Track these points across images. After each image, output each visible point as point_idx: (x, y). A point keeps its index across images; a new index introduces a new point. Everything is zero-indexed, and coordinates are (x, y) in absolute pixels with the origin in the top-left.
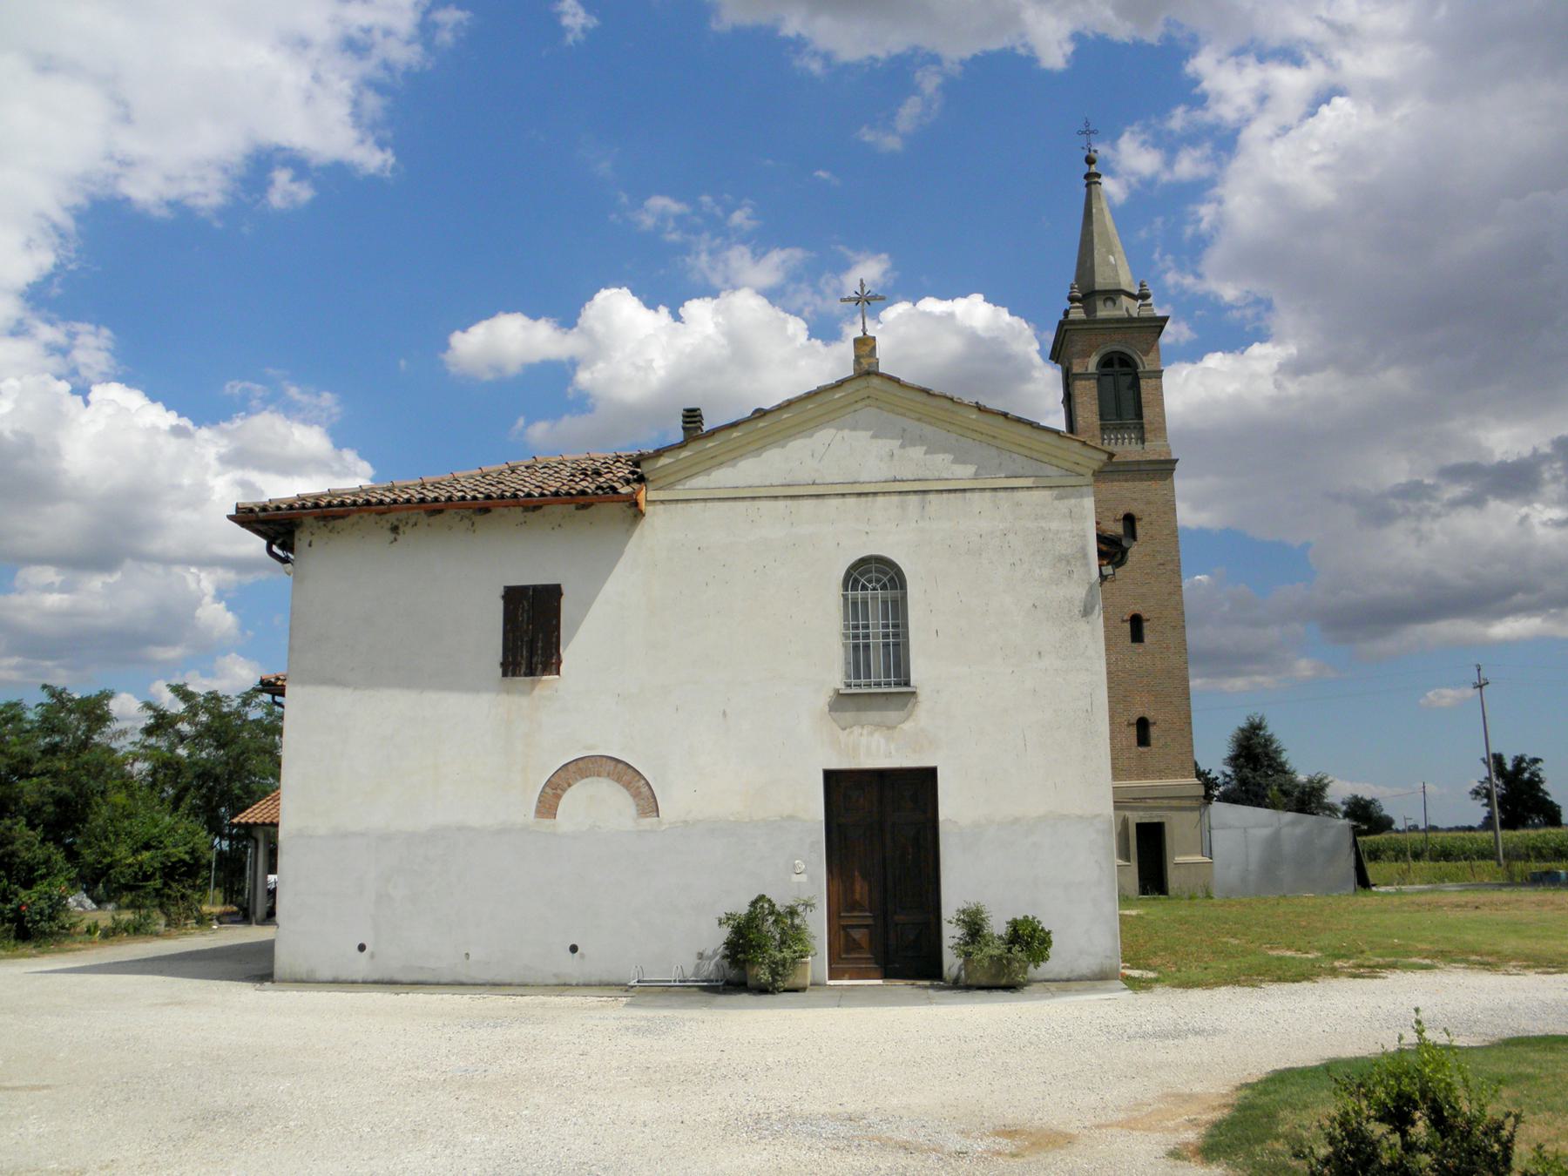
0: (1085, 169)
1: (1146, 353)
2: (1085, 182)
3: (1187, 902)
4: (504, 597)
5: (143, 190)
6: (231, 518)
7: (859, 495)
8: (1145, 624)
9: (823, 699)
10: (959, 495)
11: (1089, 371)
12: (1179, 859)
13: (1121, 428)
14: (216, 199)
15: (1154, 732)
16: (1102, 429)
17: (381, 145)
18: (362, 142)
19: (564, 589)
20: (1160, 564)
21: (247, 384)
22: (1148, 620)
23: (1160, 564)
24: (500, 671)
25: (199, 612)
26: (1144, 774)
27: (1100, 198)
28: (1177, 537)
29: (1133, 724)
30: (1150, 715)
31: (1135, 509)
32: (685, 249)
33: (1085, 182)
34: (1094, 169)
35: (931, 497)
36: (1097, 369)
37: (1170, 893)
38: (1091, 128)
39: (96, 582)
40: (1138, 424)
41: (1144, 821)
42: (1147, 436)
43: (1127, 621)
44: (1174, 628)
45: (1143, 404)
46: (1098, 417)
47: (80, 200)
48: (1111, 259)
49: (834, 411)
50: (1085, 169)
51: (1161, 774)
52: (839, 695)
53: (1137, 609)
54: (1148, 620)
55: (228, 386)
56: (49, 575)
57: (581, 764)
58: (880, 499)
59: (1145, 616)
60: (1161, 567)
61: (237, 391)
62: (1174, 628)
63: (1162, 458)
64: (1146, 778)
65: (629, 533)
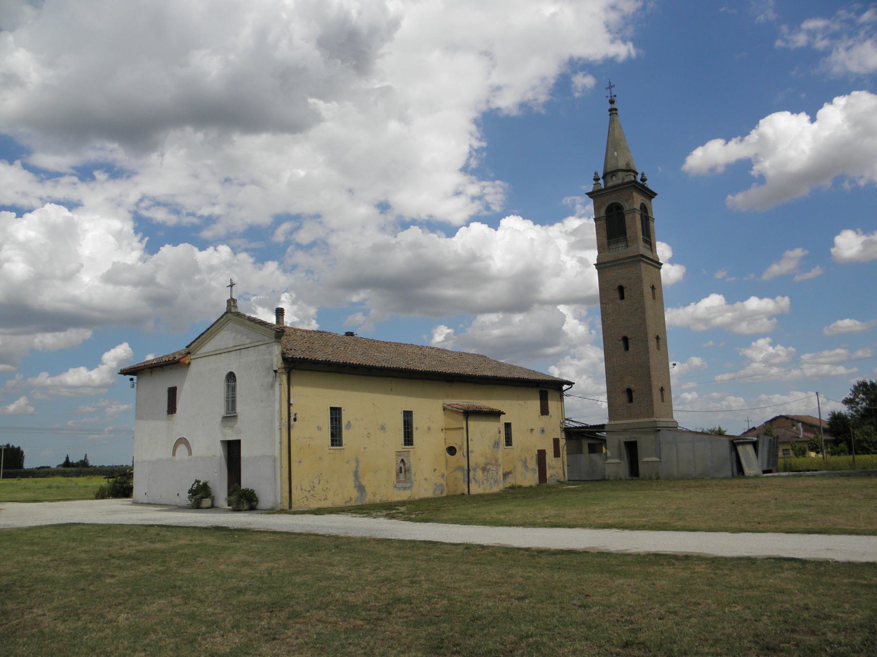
0: (609, 106)
1: (627, 201)
2: (609, 113)
3: (656, 481)
4: (168, 391)
5: (507, 102)
6: (119, 373)
7: (228, 352)
8: (629, 341)
9: (219, 419)
10: (247, 349)
11: (602, 216)
12: (645, 459)
13: (618, 242)
14: (542, 98)
15: (634, 395)
16: (608, 244)
17: (624, 41)
18: (612, 42)
19: (177, 387)
20: (636, 310)
21: (573, 198)
22: (630, 339)
23: (636, 310)
24: (167, 413)
25: (565, 327)
26: (630, 417)
27: (614, 122)
28: (643, 294)
29: (624, 392)
30: (632, 387)
31: (624, 283)
32: (827, 53)
33: (609, 113)
34: (613, 106)
35: (242, 350)
36: (606, 214)
37: (640, 477)
38: (612, 85)
39: (518, 318)
40: (625, 238)
41: (628, 440)
42: (629, 244)
43: (620, 340)
44: (642, 341)
45: (627, 228)
46: (606, 239)
47: (474, 115)
48: (616, 154)
49: (223, 325)
50: (609, 106)
51: (638, 416)
52: (224, 417)
53: (625, 333)
54: (630, 339)
55: (564, 201)
56: (493, 317)
57: (178, 441)
58: (232, 352)
59: (629, 337)
60: (636, 311)
61: (568, 202)
62: (642, 341)
63: (635, 254)
64: (631, 419)
65: (188, 369)
